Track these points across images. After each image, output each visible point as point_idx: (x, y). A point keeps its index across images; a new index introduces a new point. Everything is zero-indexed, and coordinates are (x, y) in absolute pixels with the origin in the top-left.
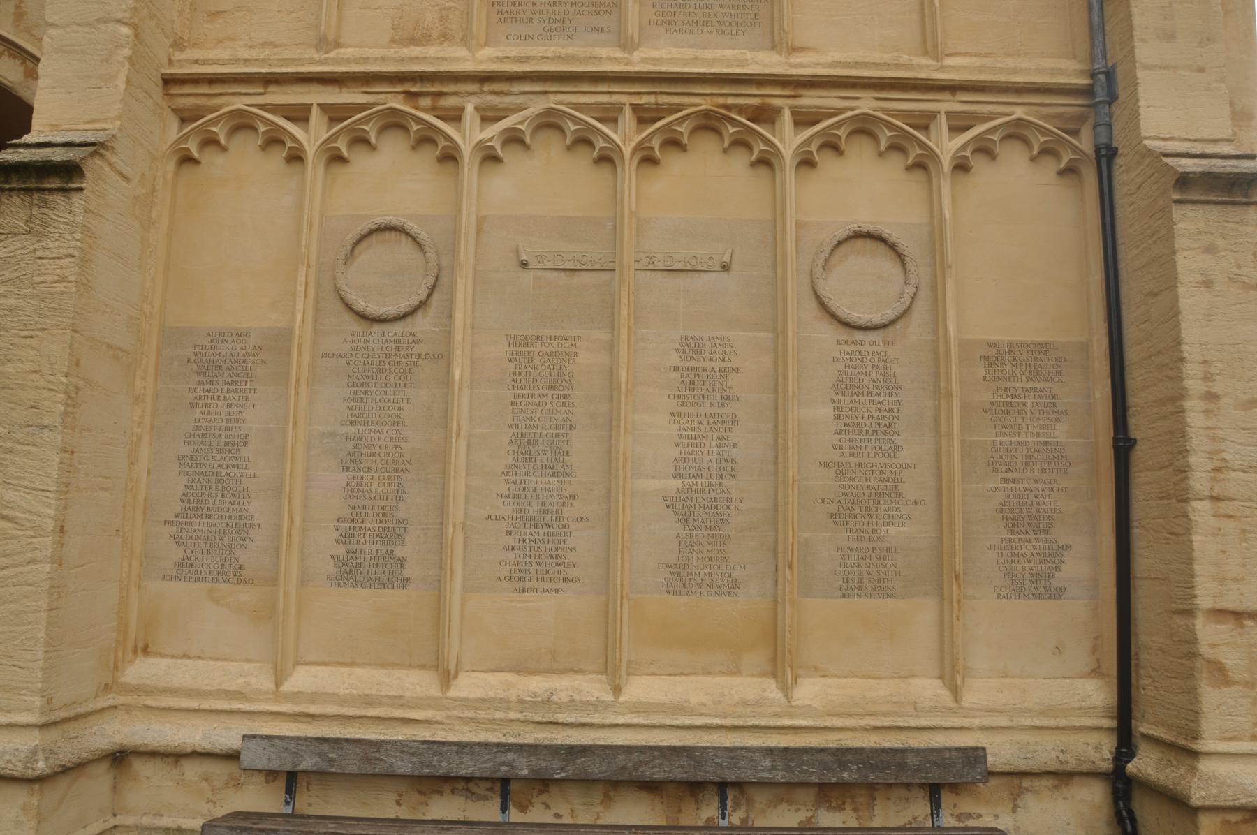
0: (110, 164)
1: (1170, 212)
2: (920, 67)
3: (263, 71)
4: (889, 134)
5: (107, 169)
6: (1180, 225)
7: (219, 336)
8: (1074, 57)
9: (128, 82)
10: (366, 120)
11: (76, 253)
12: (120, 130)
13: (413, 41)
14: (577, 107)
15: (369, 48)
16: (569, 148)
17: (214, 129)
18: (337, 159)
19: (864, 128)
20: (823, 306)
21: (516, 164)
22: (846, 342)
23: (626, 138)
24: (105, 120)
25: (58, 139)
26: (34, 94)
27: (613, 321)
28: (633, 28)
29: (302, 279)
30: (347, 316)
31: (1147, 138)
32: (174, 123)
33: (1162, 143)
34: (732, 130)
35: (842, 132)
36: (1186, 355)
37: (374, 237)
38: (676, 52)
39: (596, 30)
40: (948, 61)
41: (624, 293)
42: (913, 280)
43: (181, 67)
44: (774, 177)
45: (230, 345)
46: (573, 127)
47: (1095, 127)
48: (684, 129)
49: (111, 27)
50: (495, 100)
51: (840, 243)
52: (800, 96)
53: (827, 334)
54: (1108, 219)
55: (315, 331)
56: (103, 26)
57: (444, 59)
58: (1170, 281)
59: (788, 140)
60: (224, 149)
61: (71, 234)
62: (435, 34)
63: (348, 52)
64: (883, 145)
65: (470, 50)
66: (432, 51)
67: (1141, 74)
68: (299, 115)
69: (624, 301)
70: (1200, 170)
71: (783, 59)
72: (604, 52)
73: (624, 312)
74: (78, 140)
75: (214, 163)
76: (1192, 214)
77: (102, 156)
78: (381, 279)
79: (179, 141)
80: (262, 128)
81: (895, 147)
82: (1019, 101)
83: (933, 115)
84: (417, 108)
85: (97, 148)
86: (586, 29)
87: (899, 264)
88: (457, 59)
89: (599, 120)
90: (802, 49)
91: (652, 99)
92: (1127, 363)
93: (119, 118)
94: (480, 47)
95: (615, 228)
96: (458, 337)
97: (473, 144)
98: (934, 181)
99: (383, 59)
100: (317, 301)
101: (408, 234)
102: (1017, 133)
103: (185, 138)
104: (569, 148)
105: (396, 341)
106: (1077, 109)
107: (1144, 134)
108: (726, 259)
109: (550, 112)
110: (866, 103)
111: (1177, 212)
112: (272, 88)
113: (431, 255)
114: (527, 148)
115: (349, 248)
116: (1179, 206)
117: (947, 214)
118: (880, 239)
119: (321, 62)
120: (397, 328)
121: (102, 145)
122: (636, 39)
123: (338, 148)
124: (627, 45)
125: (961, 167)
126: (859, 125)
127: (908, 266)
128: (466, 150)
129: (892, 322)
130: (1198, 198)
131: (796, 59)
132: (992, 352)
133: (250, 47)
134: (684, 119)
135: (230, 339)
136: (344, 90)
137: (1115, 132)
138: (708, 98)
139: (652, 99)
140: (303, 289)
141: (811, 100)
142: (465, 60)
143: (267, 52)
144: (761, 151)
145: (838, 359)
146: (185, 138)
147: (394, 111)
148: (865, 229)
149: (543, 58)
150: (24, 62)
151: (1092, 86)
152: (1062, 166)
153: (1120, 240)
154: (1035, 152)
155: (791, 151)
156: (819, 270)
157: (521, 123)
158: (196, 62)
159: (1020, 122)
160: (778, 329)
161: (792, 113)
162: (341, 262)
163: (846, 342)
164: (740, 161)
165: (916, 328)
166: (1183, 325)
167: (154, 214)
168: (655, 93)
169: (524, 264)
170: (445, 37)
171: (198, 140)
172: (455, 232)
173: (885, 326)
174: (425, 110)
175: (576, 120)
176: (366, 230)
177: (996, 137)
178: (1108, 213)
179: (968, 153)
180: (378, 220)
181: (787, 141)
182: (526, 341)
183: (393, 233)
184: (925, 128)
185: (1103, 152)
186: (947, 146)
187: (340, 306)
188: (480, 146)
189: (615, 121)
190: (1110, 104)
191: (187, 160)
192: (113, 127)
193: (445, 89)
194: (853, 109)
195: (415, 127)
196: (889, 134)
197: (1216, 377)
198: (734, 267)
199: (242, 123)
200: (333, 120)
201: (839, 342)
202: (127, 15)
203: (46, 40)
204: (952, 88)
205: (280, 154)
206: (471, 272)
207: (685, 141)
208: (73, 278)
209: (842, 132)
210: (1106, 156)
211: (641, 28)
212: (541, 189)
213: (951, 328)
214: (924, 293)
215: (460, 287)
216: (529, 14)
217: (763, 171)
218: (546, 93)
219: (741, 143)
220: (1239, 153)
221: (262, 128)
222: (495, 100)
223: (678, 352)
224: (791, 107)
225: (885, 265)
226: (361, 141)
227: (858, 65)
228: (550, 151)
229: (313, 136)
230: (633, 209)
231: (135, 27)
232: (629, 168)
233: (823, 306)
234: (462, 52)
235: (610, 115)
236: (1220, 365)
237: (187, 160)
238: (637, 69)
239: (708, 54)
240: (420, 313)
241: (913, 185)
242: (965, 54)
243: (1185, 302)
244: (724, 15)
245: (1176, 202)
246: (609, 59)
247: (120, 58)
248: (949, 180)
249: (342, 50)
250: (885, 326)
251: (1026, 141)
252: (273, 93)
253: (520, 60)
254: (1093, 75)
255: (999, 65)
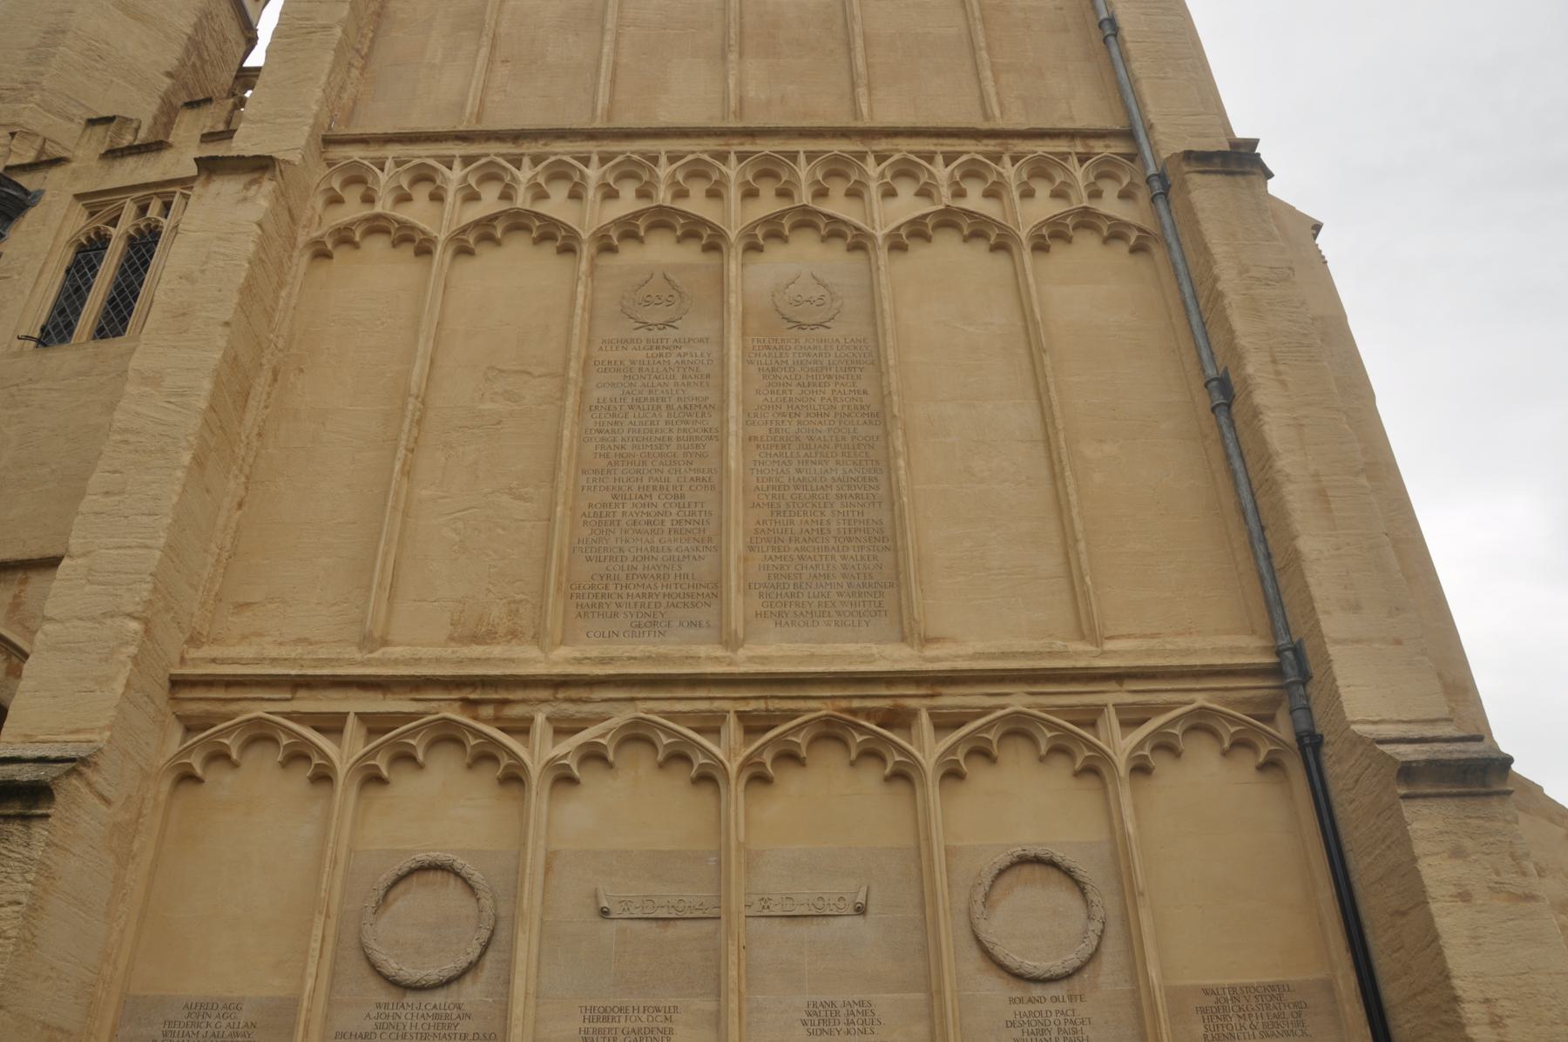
0: (89, 784)
1: (1399, 809)
2: (1077, 654)
3: (293, 672)
4: (1049, 735)
5: (85, 790)
6: (1415, 825)
7: (201, 1009)
8: (1254, 632)
9: (128, 685)
10: (413, 733)
11: (24, 899)
12: (109, 742)
13: (475, 639)
14: (670, 715)
15: (421, 647)
16: (661, 766)
17: (226, 741)
18: (373, 779)
19: (1019, 728)
20: (987, 953)
21: (597, 787)
22: (1021, 1000)
23: (731, 752)
24: (92, 730)
25: (30, 753)
26: (12, 695)
27: (719, 985)
28: (737, 622)
29: (317, 933)
30: (373, 983)
31: (1354, 722)
32: (178, 733)
33: (1372, 728)
34: (859, 739)
35: (993, 736)
36: (1460, 993)
37: (414, 879)
38: (788, 649)
39: (692, 624)
40: (1109, 646)
41: (733, 948)
42: (1098, 913)
43: (195, 666)
44: (914, 793)
45: (213, 1021)
46: (666, 741)
47: (1291, 712)
48: (801, 739)
49: (118, 621)
50: (570, 709)
51: (1001, 872)
52: (939, 695)
53: (996, 990)
54: (1327, 821)
55: (330, 1003)
56: (109, 621)
57: (512, 660)
58: (1418, 899)
59: (928, 748)
60: (235, 765)
61: (22, 874)
62: (501, 630)
63: (396, 651)
64: (1044, 749)
65: (542, 649)
66: (497, 651)
67: (1333, 650)
68: (332, 725)
69: (733, 958)
70: (1423, 757)
71: (915, 652)
72: (702, 651)
73: (733, 973)
74: (54, 754)
75: (221, 782)
76: (1426, 811)
77: (80, 774)
78: (421, 933)
79: (179, 755)
80: (285, 741)
81: (1058, 750)
82: (1198, 686)
83: (1099, 710)
84: (475, 718)
85: (75, 765)
86: (681, 624)
87: (1078, 894)
88: (526, 661)
89: (698, 731)
90: (937, 640)
91: (761, 705)
92: (1386, 1005)
93: (110, 727)
94: (555, 646)
95: (719, 863)
96: (517, 1010)
97: (543, 762)
98: (1110, 787)
99: (438, 660)
100: (335, 962)
101: (457, 874)
102: (1201, 723)
103: (188, 751)
104: (661, 766)
105: (435, 1016)
106: (1266, 692)
107: (1350, 717)
108: (861, 898)
109: (638, 722)
110: (1018, 700)
111: (1408, 810)
112: (301, 693)
113: (487, 902)
114: (610, 766)
115: (382, 893)
116: (1408, 802)
117: (1130, 828)
118: (1051, 863)
119: (363, 664)
120: (438, 998)
121: (83, 761)
122: (741, 635)
123: (376, 767)
124: (730, 642)
125: (1141, 769)
126: (1012, 726)
127: (1090, 896)
128: (535, 769)
129: (1078, 970)
130: (1428, 791)
131: (930, 652)
132: (1210, 1001)
133: (281, 644)
134: (800, 727)
135: (214, 1013)
136: (389, 696)
137: (1316, 717)
138: (829, 702)
139: (761, 705)
140: (317, 945)
141: (952, 699)
142: (536, 661)
143: (298, 651)
144: (897, 763)
145: (1013, 1024)
146: (188, 751)
147: (447, 722)
148: (1031, 852)
149: (630, 658)
150: (8, 658)
151: (1279, 664)
152: (1261, 759)
153: (1347, 847)
154: (1227, 745)
155: (932, 761)
156: (978, 908)
157: (603, 736)
158: (214, 661)
159: (1202, 711)
160: (931, 986)
161: (932, 716)
162: (370, 910)
163: (1021, 1000)
164: (871, 777)
165: (1109, 975)
166: (1448, 952)
167: (136, 846)
168: (765, 698)
169: (604, 913)
170: (513, 635)
171: (204, 754)
172: (518, 871)
173: (1068, 976)
174: (485, 721)
175: (669, 732)
176: (405, 869)
177: (1177, 731)
178: (1325, 814)
179: (1146, 752)
180: (421, 856)
181: (927, 746)
182: (606, 1014)
183: (439, 874)
184: (1092, 725)
185: (1307, 740)
186: (1121, 745)
187: (364, 968)
188: (552, 764)
189: (717, 731)
190: (1304, 684)
191: (187, 777)
192: (101, 739)
193: (511, 696)
194: (1003, 707)
195: (473, 742)
196: (1049, 735)
197: (1508, 1021)
198: (871, 909)
199: (260, 734)
200: (372, 732)
201: (1012, 1001)
202: (140, 608)
203: (39, 636)
204: (1118, 676)
205: (304, 772)
206: (536, 923)
207: (803, 753)
208: (13, 933)
209: (993, 736)
210: (1310, 745)
211: (746, 622)
212: (632, 813)
213: (1154, 973)
214: (1114, 929)
215: (522, 943)
216: (613, 608)
217: (900, 786)
218: (632, 699)
219: (871, 754)
220: (1462, 734)
221: (285, 741)
222: (570, 709)
223: (804, 1023)
224: (929, 708)
225: (1062, 896)
226: (405, 757)
227: (1004, 655)
228: (637, 770)
229: (345, 753)
230: (742, 839)
231: (146, 622)
232: (736, 789)
233: (987, 953)
234: (532, 652)
235: (711, 725)
236: (1505, 1003)
237: (187, 777)
238: (742, 669)
239: (827, 649)
240: (468, 978)
241: (1084, 796)
242: (1129, 636)
243: (1443, 923)
244: (843, 603)
245: (1404, 797)
246: (709, 658)
247: (122, 658)
248: (1127, 786)
249: (389, 649)
250: (1068, 976)
251: (1214, 734)
252: (302, 699)
253: (603, 661)
254: (1279, 653)
255: (1169, 647)
